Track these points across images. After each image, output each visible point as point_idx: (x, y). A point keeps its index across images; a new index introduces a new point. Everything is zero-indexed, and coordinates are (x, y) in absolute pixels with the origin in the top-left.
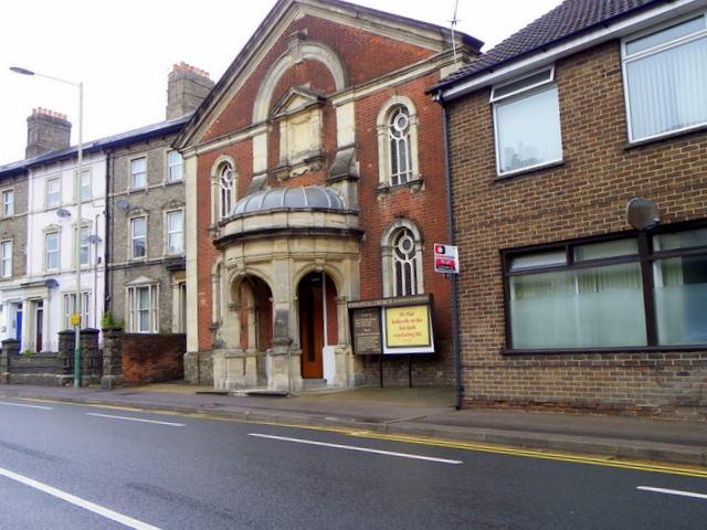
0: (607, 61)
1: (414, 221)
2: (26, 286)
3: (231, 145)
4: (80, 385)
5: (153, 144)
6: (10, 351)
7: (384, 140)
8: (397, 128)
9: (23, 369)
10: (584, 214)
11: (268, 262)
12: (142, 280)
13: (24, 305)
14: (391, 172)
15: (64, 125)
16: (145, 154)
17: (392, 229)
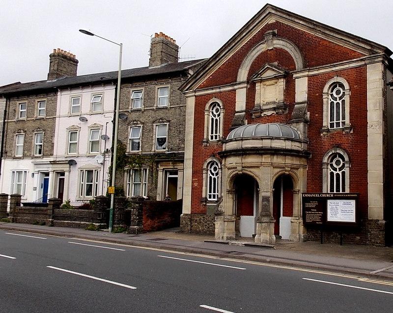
1: (345, 150)
2: (53, 163)
3: (220, 92)
4: (112, 231)
6: (54, 205)
7: (327, 102)
9: (65, 217)
11: (258, 167)
13: (50, 175)
14: (329, 121)
15: (74, 62)
17: (330, 153)
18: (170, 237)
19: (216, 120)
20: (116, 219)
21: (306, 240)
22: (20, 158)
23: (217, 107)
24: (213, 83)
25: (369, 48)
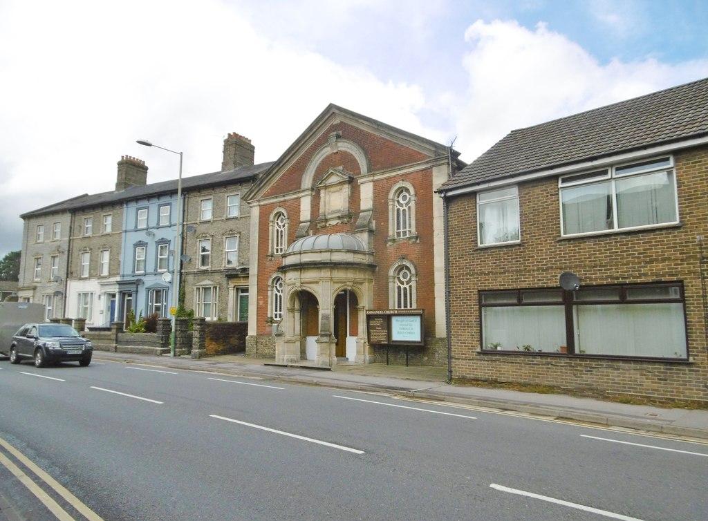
0: (550, 187)
3: (285, 201)
4: (175, 355)
5: (217, 190)
8: (401, 201)
10: (532, 275)
11: (317, 282)
12: (207, 282)
16: (212, 197)
18: (231, 362)
19: (281, 231)
20: (178, 342)
21: (372, 362)
22: (86, 279)
23: (282, 217)
24: (275, 192)
25: (433, 149)
